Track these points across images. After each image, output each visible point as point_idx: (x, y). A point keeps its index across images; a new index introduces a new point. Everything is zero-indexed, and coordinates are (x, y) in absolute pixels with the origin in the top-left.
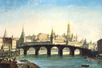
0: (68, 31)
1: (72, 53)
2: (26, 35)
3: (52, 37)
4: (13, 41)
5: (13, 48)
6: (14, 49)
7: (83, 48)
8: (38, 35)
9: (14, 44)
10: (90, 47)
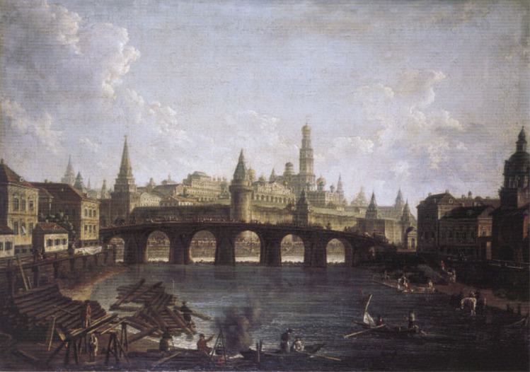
0: (305, 158)
1: (225, 255)
2: (140, 178)
3: (238, 188)
4: (86, 207)
5: (85, 236)
6: (90, 243)
7: (491, 225)
8: (188, 182)
9: (89, 216)
10: (393, 236)
